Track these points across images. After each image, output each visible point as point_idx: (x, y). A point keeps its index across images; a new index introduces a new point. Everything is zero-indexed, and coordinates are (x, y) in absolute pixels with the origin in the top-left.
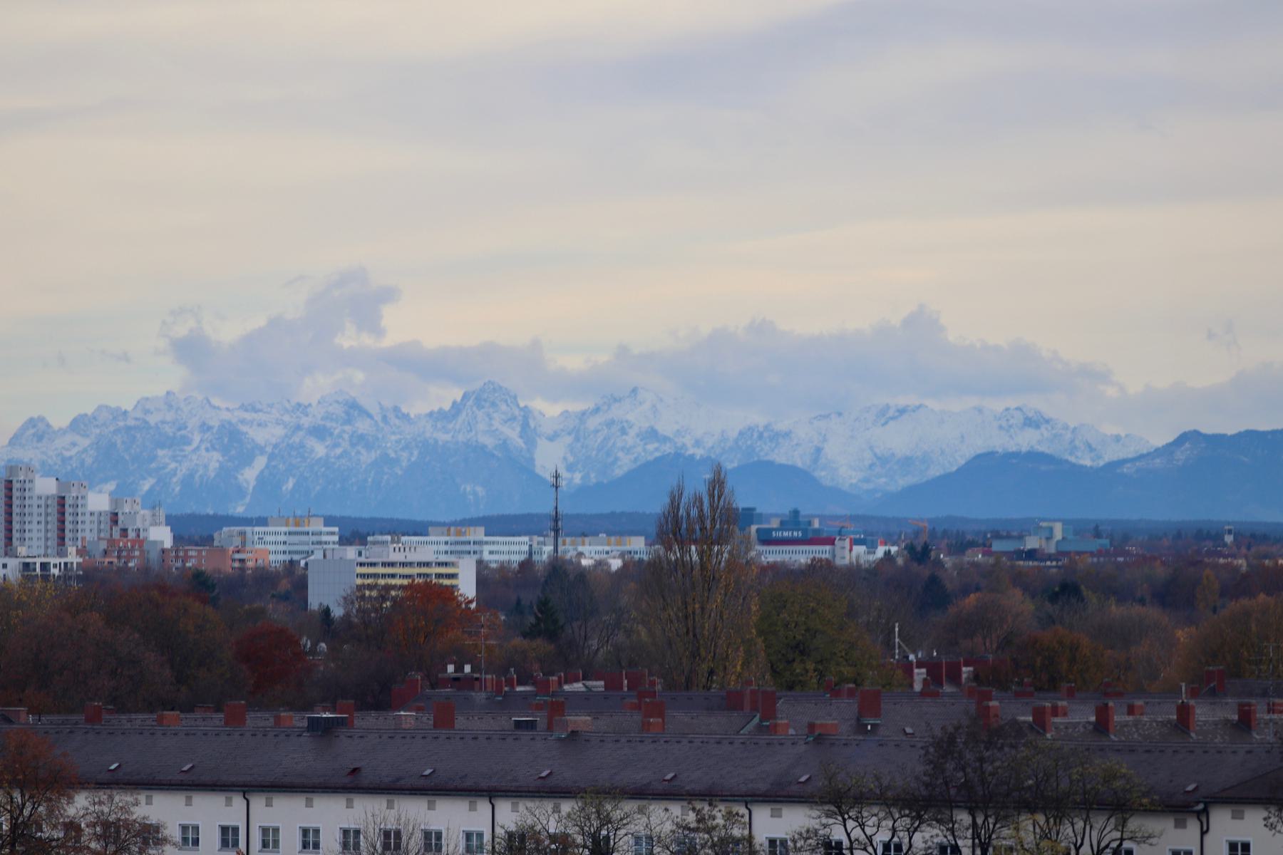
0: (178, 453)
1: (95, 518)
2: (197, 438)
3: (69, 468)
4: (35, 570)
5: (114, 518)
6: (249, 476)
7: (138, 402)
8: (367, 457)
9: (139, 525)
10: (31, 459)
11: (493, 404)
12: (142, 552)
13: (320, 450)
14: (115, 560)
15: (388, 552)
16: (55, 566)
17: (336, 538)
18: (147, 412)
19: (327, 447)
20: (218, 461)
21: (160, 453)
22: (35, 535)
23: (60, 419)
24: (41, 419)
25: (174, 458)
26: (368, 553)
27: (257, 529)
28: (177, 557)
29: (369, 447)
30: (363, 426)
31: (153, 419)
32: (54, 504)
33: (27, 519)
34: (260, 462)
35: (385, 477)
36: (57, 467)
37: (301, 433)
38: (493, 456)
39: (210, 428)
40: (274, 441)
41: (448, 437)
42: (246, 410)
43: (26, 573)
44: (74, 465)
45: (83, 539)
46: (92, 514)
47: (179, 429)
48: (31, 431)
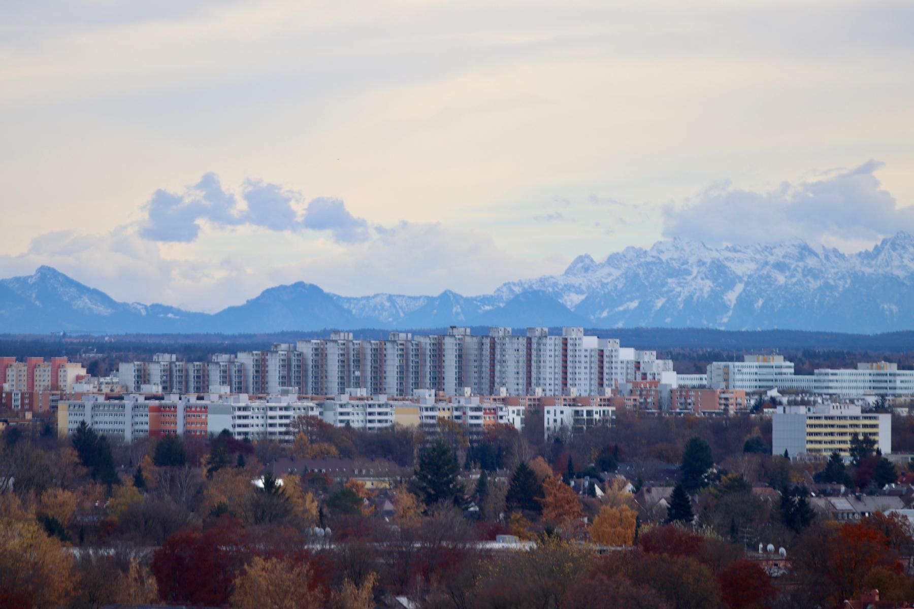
0: (682, 281)
1: (624, 365)
2: (695, 271)
3: (606, 290)
4: (582, 415)
5: (638, 365)
6: (731, 297)
7: (654, 245)
8: (814, 284)
9: (655, 370)
10: (580, 284)
11: (904, 248)
12: (656, 391)
13: (781, 279)
14: (638, 398)
15: (829, 409)
16: (596, 413)
17: (792, 370)
18: (661, 252)
19: (786, 277)
20: (710, 286)
21: (670, 280)
22: (583, 376)
23: (599, 256)
24: (587, 256)
25: (679, 284)
26: (814, 409)
27: (737, 364)
28: (681, 395)
29: (816, 277)
30: (811, 262)
31: (664, 257)
32: (596, 355)
33: (578, 365)
34: (739, 288)
35: (827, 299)
36: (598, 290)
37: (768, 268)
38: (904, 284)
39: (704, 264)
40: (749, 273)
41: (871, 271)
42: (730, 251)
43: (577, 417)
44: (610, 289)
45: (616, 380)
46: (622, 362)
47: (683, 264)
48: (580, 265)
